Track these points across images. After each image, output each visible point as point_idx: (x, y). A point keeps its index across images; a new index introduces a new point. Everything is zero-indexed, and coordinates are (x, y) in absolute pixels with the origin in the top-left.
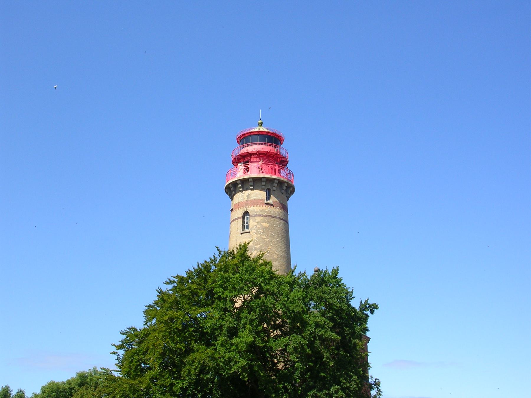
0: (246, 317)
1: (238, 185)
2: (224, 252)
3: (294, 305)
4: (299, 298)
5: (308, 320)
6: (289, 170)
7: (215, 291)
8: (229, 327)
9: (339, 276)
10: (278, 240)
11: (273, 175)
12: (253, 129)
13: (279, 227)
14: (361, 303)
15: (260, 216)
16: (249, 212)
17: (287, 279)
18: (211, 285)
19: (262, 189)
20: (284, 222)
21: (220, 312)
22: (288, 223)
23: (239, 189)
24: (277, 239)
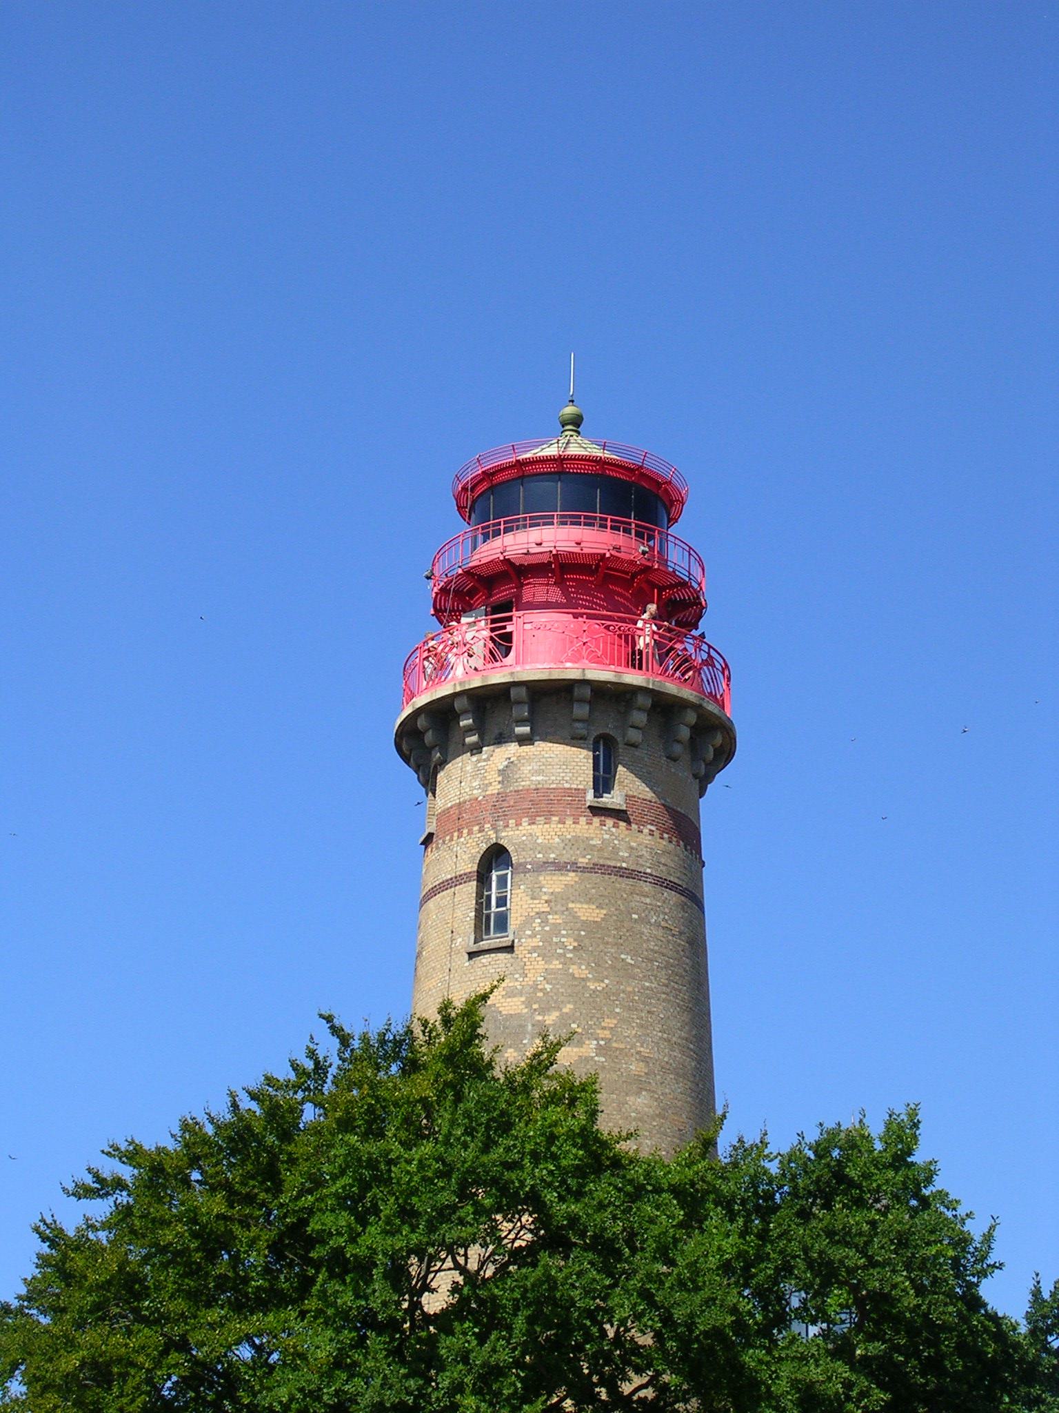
0: (465, 1358)
1: (457, 717)
2: (365, 1039)
3: (698, 1299)
4: (729, 1261)
5: (764, 1376)
6: (705, 647)
7: (318, 1227)
8: (381, 1403)
9: (919, 1157)
10: (648, 988)
11: (630, 669)
12: (537, 446)
13: (658, 925)
14: (1037, 1293)
15: (560, 867)
16: (510, 849)
17: (669, 1172)
18: (297, 1198)
19: (575, 740)
20: (683, 898)
21: (338, 1331)
22: (699, 904)
23: (464, 740)
24: (647, 984)
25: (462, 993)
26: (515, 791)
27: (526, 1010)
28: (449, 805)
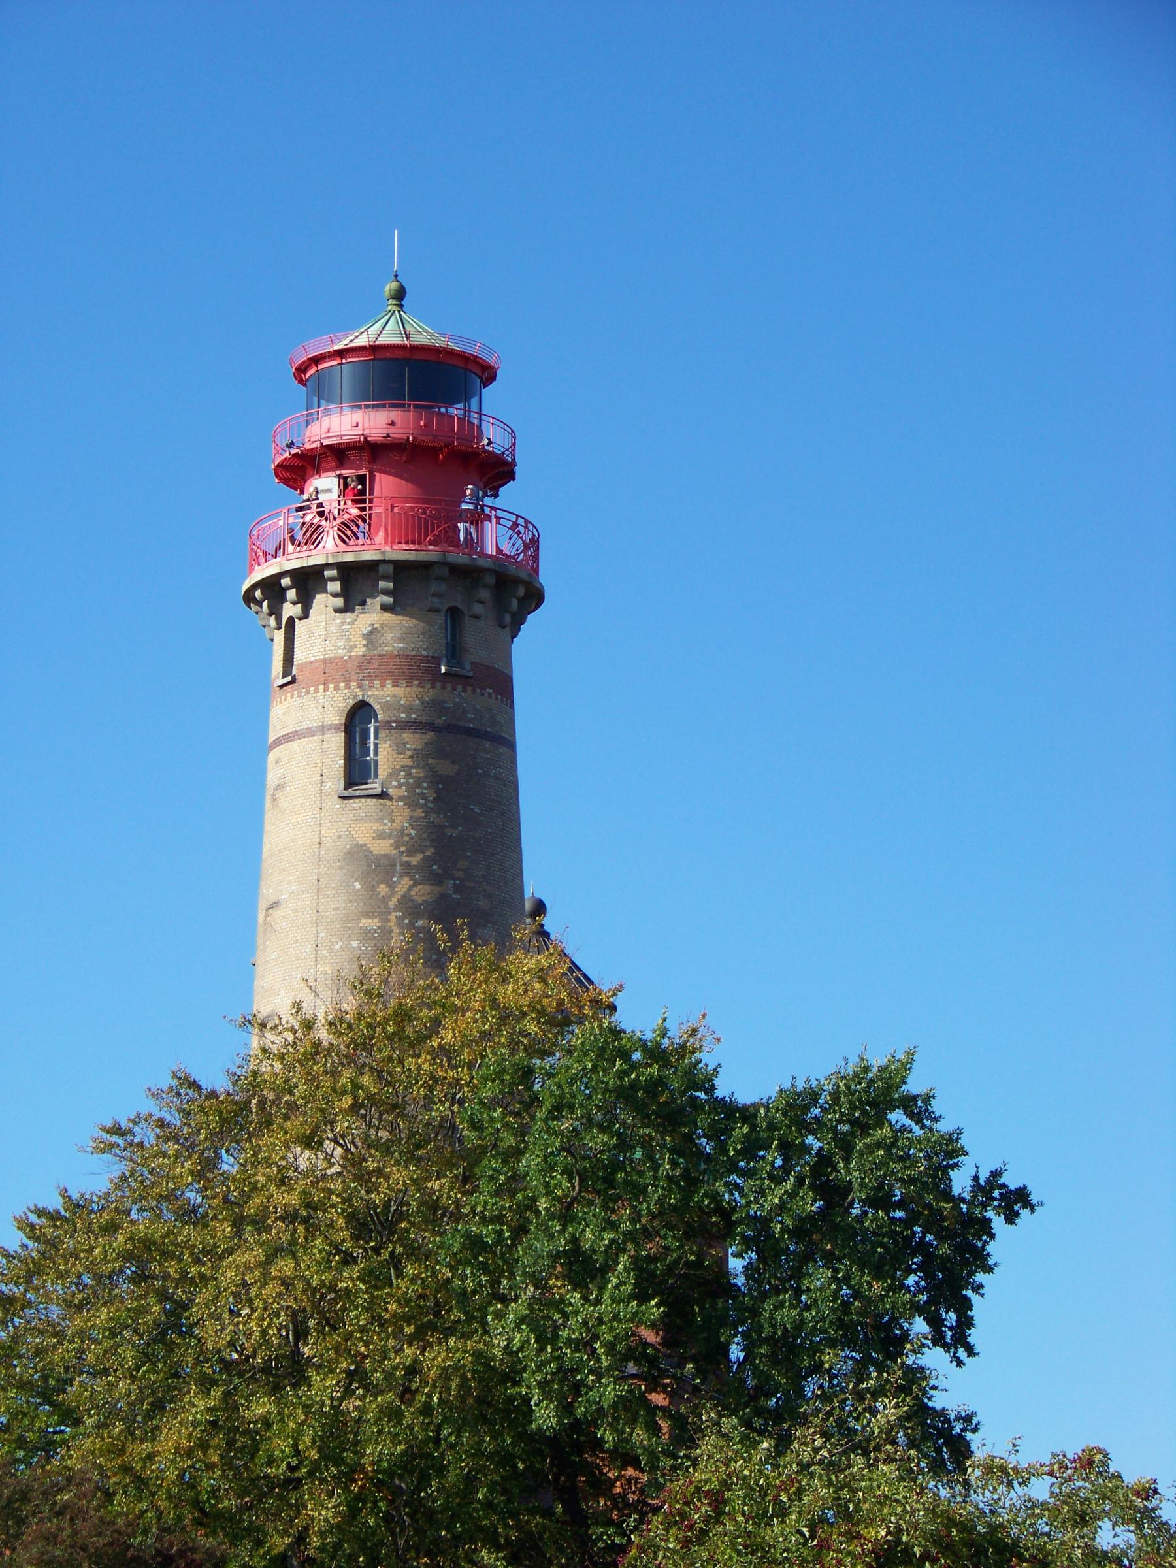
14: (976, 1178)
16: (376, 707)
25: (334, 831)
26: (379, 655)
27: (395, 852)
28: (313, 659)
